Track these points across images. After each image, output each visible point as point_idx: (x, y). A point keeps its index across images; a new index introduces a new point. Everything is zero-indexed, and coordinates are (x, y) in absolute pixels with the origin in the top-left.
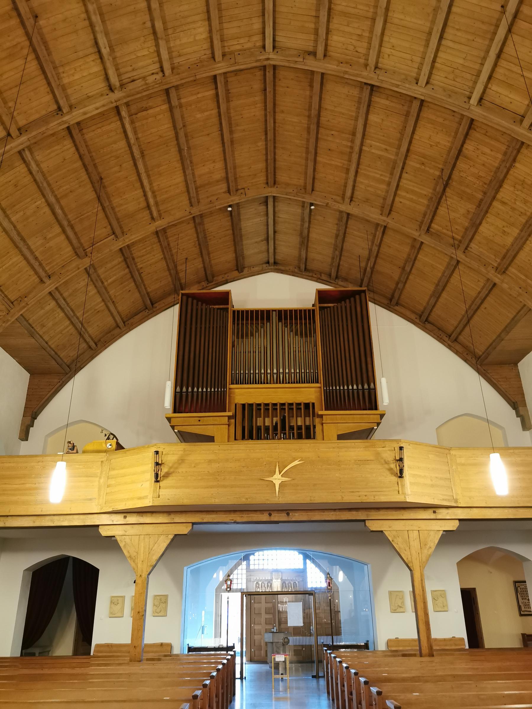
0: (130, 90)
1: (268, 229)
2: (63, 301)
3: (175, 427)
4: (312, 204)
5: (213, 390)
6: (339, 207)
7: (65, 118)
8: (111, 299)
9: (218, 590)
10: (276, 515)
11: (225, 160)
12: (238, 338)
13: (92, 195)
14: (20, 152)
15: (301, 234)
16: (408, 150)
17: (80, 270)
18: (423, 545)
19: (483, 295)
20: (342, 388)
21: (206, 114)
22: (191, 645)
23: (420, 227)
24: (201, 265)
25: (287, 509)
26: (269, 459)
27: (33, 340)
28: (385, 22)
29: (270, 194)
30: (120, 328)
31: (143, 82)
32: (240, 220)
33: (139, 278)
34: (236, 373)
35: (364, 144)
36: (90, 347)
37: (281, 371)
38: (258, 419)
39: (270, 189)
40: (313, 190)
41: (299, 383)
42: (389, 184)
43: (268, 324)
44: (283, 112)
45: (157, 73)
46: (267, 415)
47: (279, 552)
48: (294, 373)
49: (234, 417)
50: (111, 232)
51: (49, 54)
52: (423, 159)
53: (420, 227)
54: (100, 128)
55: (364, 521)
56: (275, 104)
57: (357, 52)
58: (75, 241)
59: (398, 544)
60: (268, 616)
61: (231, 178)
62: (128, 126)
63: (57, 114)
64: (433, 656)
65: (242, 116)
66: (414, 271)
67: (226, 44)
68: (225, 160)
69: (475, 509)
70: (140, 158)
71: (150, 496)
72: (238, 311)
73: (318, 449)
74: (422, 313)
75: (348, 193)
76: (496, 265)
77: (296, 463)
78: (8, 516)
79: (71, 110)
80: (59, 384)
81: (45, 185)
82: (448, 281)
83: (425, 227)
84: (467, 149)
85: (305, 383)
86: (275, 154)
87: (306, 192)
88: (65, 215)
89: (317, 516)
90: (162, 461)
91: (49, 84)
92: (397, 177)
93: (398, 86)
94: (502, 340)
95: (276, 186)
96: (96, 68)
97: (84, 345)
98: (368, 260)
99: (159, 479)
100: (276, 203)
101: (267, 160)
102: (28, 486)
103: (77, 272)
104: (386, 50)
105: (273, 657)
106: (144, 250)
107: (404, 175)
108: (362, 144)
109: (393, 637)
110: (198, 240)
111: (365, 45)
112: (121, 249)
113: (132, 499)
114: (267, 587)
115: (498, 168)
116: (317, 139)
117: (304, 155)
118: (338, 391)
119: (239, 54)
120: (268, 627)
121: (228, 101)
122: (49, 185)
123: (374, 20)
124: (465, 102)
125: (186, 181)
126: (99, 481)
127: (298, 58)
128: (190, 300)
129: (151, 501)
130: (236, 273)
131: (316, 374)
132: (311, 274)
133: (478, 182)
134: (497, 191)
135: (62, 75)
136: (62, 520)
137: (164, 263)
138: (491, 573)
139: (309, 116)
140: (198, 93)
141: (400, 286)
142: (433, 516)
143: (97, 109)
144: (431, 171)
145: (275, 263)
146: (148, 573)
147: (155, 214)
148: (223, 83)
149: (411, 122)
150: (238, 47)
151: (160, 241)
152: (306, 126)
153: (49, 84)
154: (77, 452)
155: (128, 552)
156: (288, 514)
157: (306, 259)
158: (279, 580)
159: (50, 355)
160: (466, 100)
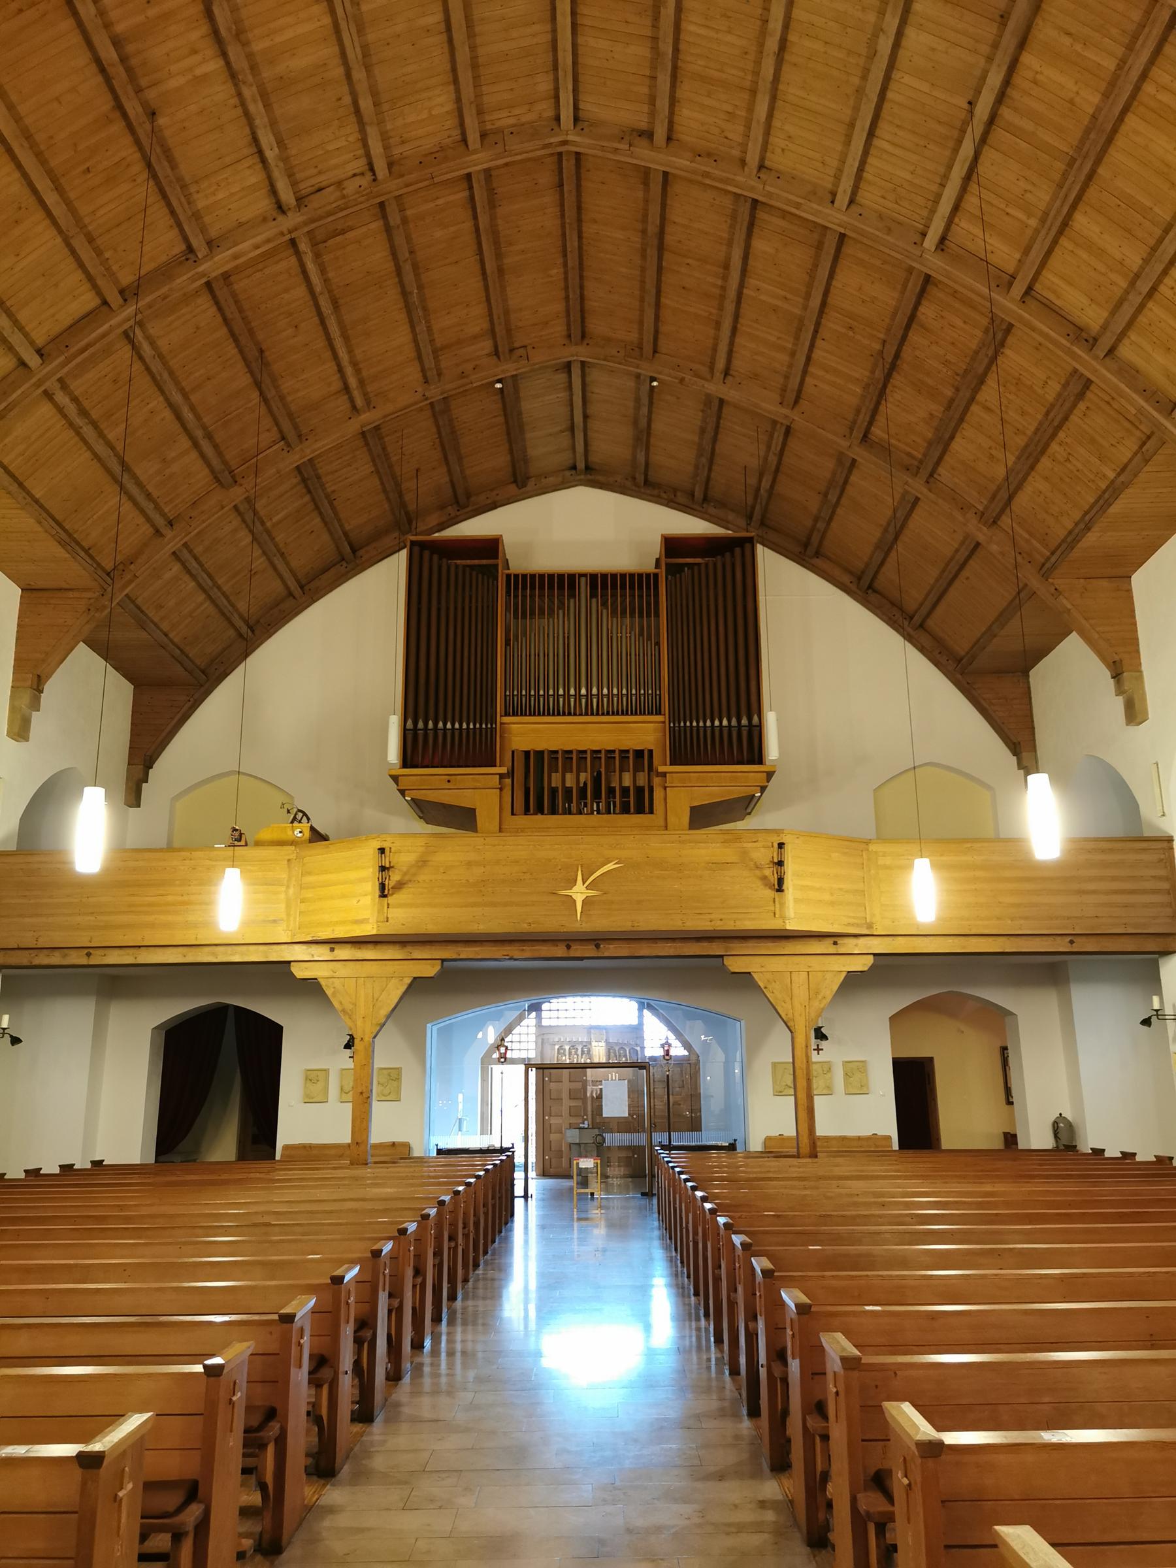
0: (315, 210)
1: (572, 411)
2: (194, 564)
3: (407, 792)
4: (653, 379)
5: (471, 726)
6: (703, 386)
7: (201, 269)
8: (279, 550)
9: (486, 1061)
10: (578, 947)
11: (488, 300)
12: (516, 617)
13: (245, 380)
14: (126, 334)
15: (635, 422)
16: (824, 304)
17: (226, 509)
18: (813, 993)
19: (961, 556)
20: (701, 724)
21: (452, 229)
22: (442, 1146)
23: (851, 430)
24: (447, 479)
25: (596, 940)
26: (566, 860)
27: (144, 635)
28: (774, 98)
29: (575, 358)
30: (294, 598)
31: (338, 194)
32: (518, 399)
33: (330, 511)
34: (513, 695)
35: (746, 285)
36: (240, 635)
37: (595, 691)
38: (553, 774)
39: (573, 349)
40: (655, 351)
41: (627, 714)
42: (793, 354)
43: (572, 601)
44: (595, 221)
45: (362, 174)
46: (567, 768)
47: (593, 999)
48: (618, 695)
49: (511, 774)
50: (279, 436)
51: (174, 166)
52: (851, 321)
53: (851, 430)
54: (261, 270)
55: (722, 956)
56: (579, 208)
57: (727, 138)
58: (215, 462)
59: (775, 993)
60: (574, 1103)
61: (500, 330)
62: (311, 266)
63: (187, 259)
64: (816, 1157)
65: (518, 229)
66: (844, 501)
67: (487, 118)
68: (488, 300)
69: (900, 938)
70: (332, 314)
71: (373, 919)
72: (516, 576)
73: (647, 844)
74: (863, 572)
75: (721, 364)
76: (981, 508)
77: (610, 866)
78: (140, 947)
79: (211, 251)
80: (189, 704)
81: (166, 375)
82: (903, 526)
83: (858, 434)
84: (924, 314)
85: (636, 714)
86: (582, 287)
87: (642, 355)
88: (198, 417)
89: (645, 949)
90: (390, 862)
91: (173, 212)
92: (807, 344)
93: (798, 206)
94: (995, 636)
95: (585, 342)
96: (255, 177)
97: (231, 633)
98: (761, 475)
99: (386, 892)
100: (586, 368)
101: (567, 298)
102: (170, 898)
103: (219, 514)
104: (777, 140)
105: (575, 1162)
106: (340, 461)
107: (819, 342)
108: (742, 285)
109: (774, 1133)
110: (440, 437)
111: (741, 129)
112: (298, 468)
113: (343, 923)
114: (582, 1054)
115: (976, 353)
116: (660, 269)
117: (637, 292)
118: (695, 729)
119: (512, 133)
120: (574, 1120)
121: (492, 204)
122: (171, 373)
123: (753, 92)
124: (915, 243)
125: (416, 341)
126: (286, 893)
127: (619, 142)
128: (426, 554)
129: (375, 926)
130: (513, 488)
131: (658, 697)
132: (656, 492)
133: (945, 370)
134: (976, 390)
135: (195, 196)
136: (229, 952)
137: (377, 482)
138: (963, 1032)
139: (644, 232)
140: (438, 198)
141: (821, 525)
142: (832, 949)
143: (257, 247)
144: (866, 342)
145: (588, 468)
146: (373, 1036)
147: (359, 402)
148: (483, 183)
149: (826, 264)
150: (512, 121)
151: (367, 444)
152: (639, 246)
153: (173, 212)
154: (246, 845)
155: (341, 1003)
156: (597, 946)
157: (647, 464)
158: (603, 1044)
159: (173, 657)
160: (917, 238)
